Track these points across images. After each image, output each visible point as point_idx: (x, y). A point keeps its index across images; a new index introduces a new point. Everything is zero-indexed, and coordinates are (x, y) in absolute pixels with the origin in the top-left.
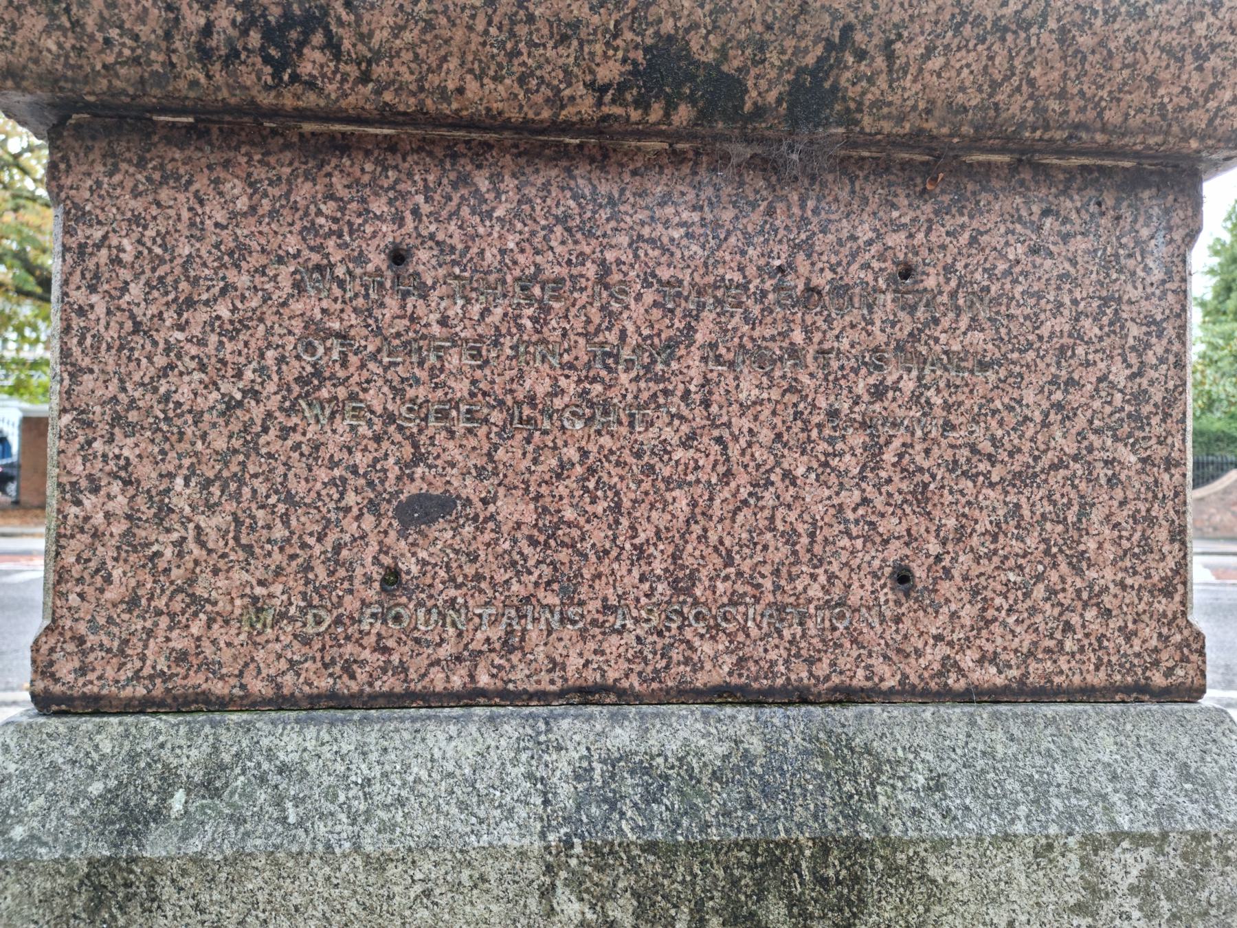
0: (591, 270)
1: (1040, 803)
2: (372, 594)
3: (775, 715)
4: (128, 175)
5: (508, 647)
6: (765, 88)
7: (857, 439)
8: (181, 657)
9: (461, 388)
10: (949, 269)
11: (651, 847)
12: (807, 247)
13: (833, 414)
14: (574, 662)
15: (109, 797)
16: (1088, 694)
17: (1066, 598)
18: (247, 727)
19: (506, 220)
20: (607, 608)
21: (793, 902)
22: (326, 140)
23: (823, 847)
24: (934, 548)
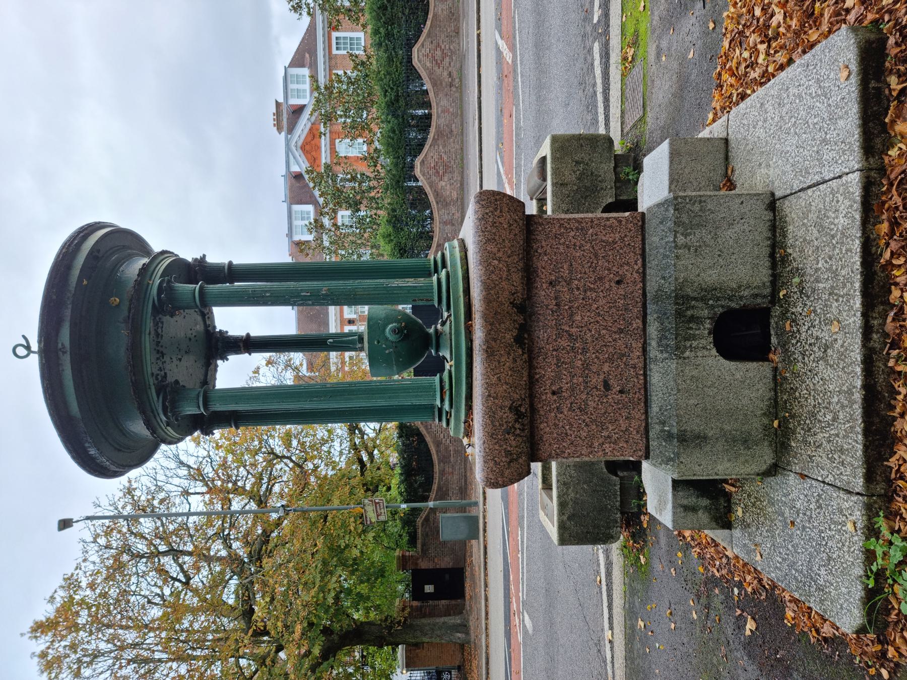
0: (554, 353)
1: (668, 257)
2: (624, 396)
3: (649, 311)
4: (541, 447)
5: (635, 368)
6: (520, 319)
7: (589, 293)
8: (638, 432)
9: (581, 379)
10: (550, 274)
11: (676, 338)
12: (547, 306)
13: (583, 299)
14: (638, 353)
15: (665, 441)
16: (643, 240)
17: (623, 245)
18: (652, 418)
19: (547, 371)
20: (626, 347)
21: (687, 309)
22: (533, 409)
23: (676, 304)
24: (612, 276)
